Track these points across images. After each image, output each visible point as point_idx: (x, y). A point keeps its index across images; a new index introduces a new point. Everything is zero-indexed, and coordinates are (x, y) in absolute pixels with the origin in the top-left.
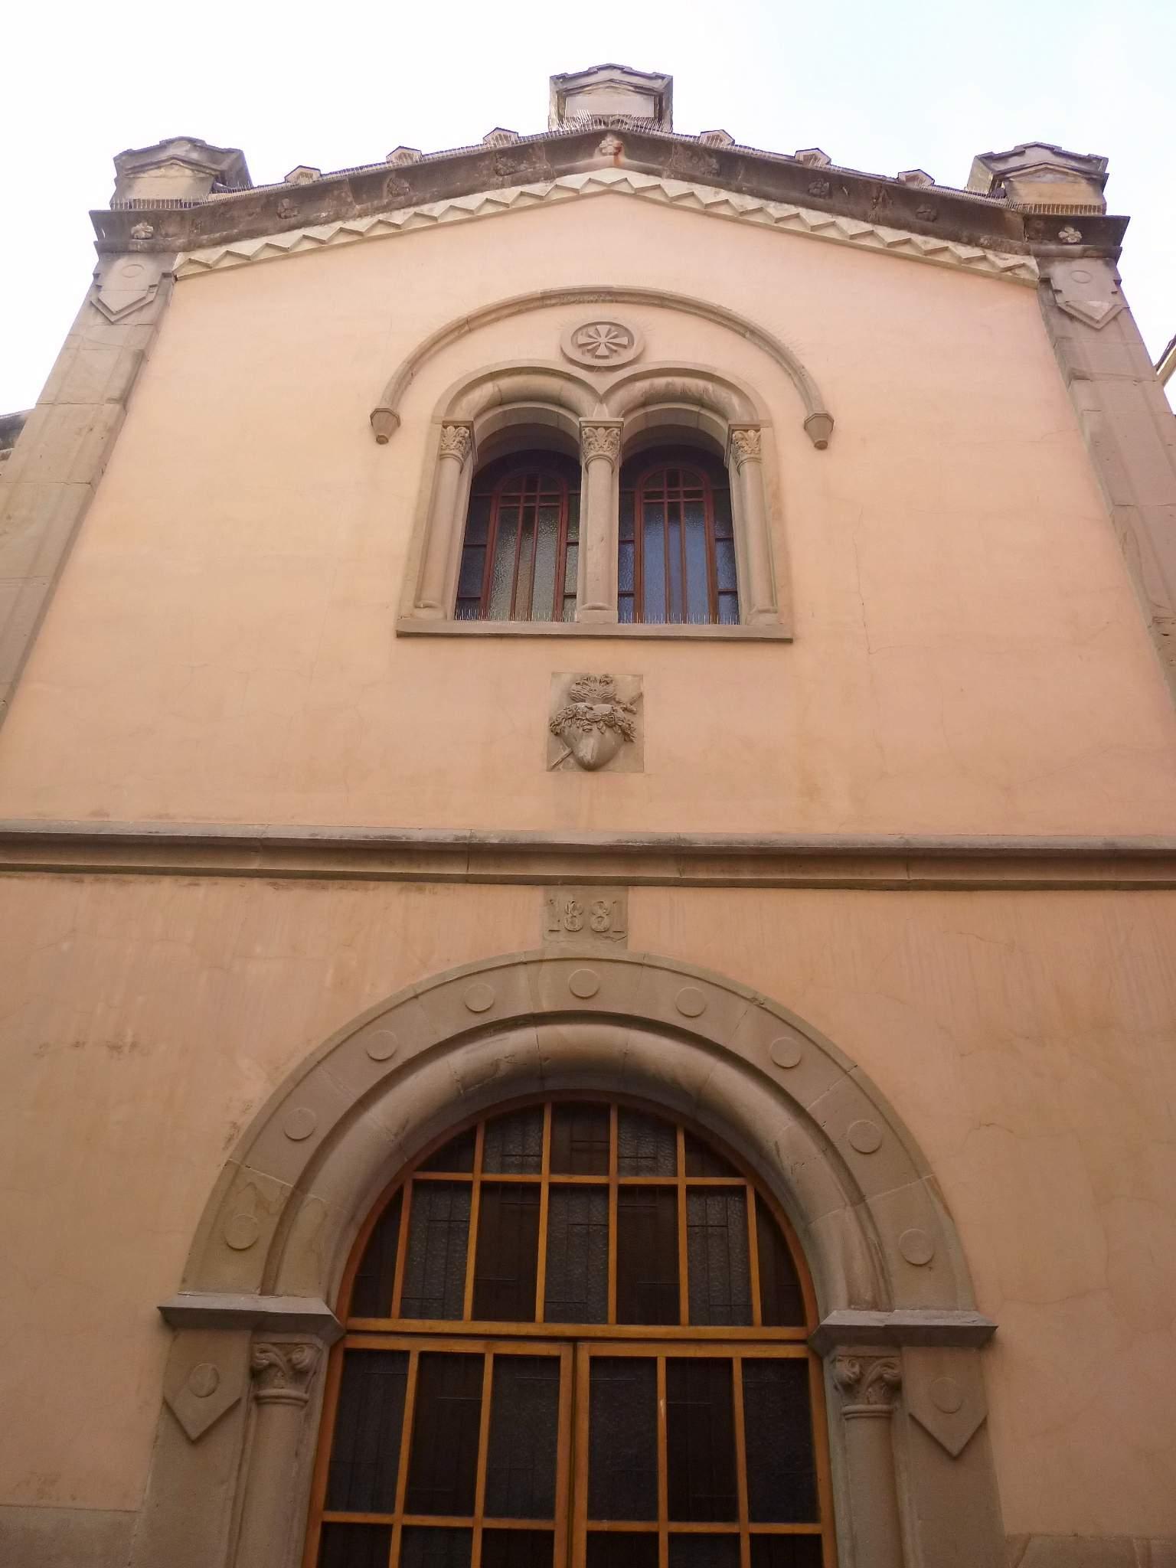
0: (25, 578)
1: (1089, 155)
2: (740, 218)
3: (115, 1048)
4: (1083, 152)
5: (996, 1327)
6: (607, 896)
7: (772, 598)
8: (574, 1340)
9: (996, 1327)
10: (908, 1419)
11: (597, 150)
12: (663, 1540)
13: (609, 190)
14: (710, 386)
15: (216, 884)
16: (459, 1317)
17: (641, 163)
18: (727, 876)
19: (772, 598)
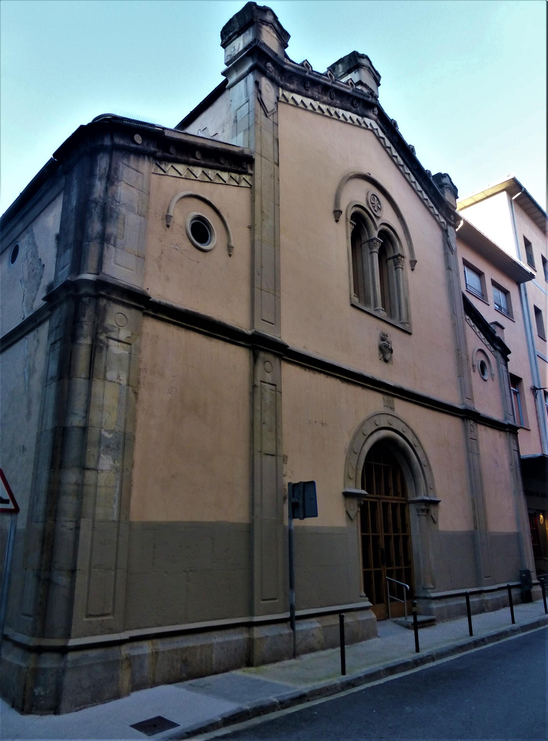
0: (261, 240)
1: (264, 6)
2: (397, 165)
3: (322, 424)
4: (455, 184)
5: (440, 501)
6: (391, 398)
7: (408, 320)
8: (378, 499)
9: (440, 501)
10: (430, 516)
11: (372, 110)
12: (371, 536)
13: (372, 131)
14: (394, 235)
15: (328, 377)
16: (373, 494)
17: (381, 125)
18: (175, 321)
19: (408, 320)
